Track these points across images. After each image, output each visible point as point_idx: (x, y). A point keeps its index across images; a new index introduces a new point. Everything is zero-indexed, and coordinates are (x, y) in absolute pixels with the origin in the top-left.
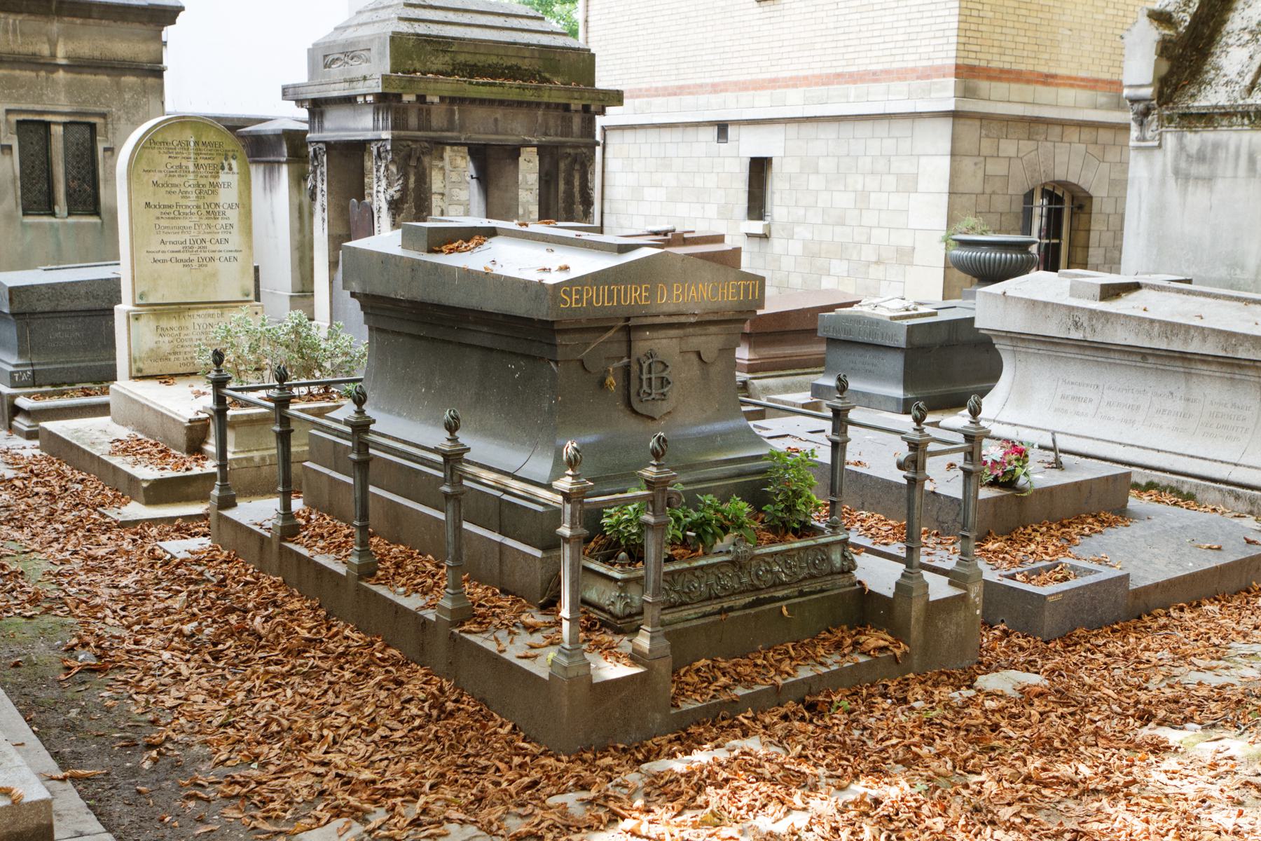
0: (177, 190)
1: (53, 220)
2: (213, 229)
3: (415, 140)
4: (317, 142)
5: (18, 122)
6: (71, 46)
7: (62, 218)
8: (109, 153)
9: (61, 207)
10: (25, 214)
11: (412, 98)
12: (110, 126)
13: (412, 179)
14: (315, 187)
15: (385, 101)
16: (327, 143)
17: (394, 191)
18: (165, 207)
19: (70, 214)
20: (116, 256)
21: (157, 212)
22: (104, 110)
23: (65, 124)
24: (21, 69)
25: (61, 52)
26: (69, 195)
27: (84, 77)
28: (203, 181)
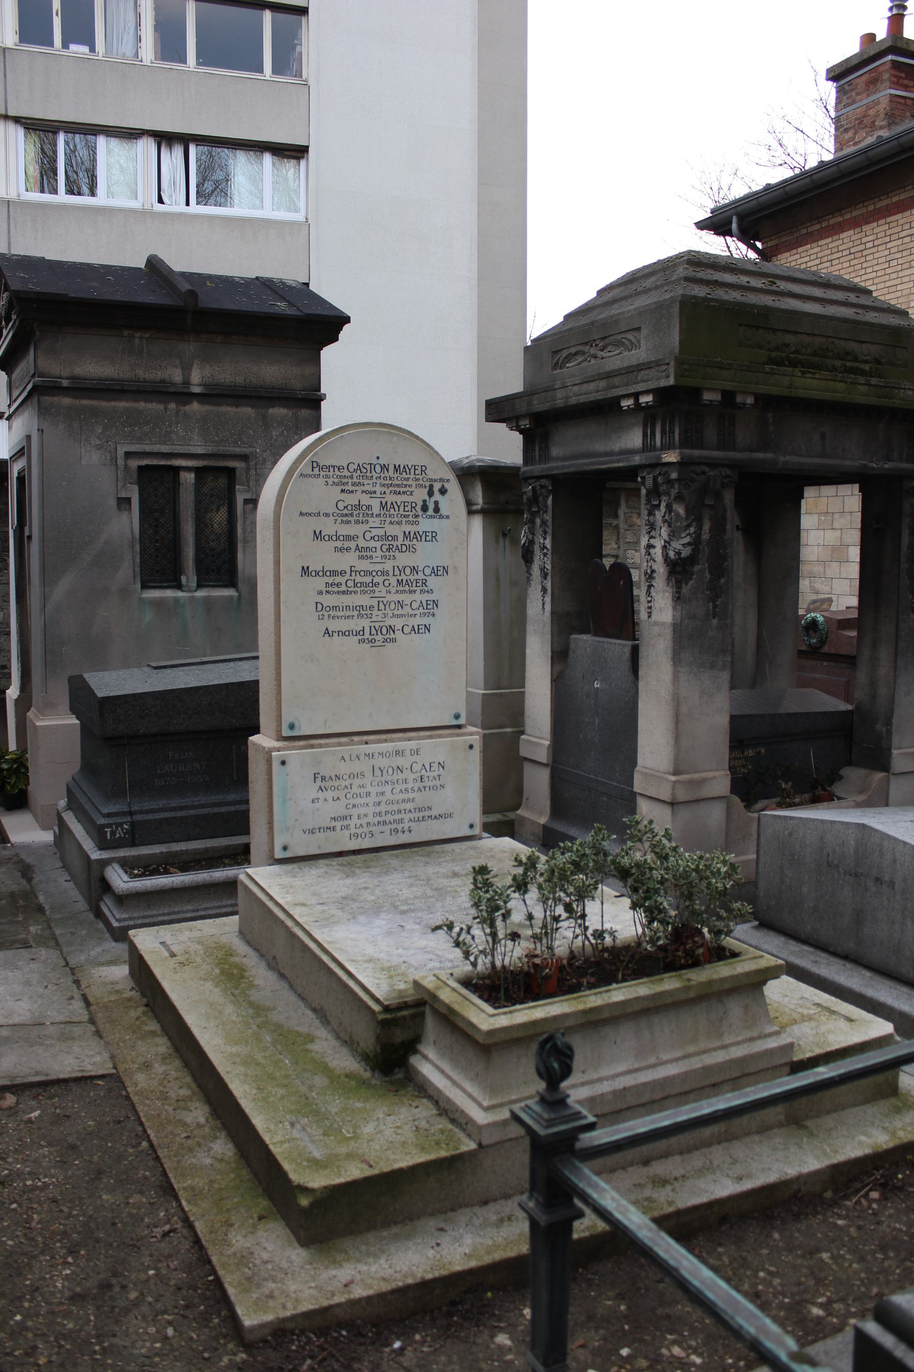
0: (352, 544)
1: (179, 594)
2: (407, 610)
3: (713, 464)
4: (538, 478)
5: (140, 468)
6: (208, 371)
7: (191, 594)
8: (250, 506)
9: (189, 577)
10: (144, 587)
11: (716, 397)
12: (253, 472)
13: (707, 526)
14: (532, 542)
15: (675, 405)
16: (553, 478)
17: (681, 546)
18: (334, 573)
19: (200, 586)
20: (254, 646)
21: (319, 583)
22: (247, 450)
23: (198, 471)
24: (146, 401)
25: (196, 377)
26: (198, 561)
27: (224, 409)
28: (393, 530)
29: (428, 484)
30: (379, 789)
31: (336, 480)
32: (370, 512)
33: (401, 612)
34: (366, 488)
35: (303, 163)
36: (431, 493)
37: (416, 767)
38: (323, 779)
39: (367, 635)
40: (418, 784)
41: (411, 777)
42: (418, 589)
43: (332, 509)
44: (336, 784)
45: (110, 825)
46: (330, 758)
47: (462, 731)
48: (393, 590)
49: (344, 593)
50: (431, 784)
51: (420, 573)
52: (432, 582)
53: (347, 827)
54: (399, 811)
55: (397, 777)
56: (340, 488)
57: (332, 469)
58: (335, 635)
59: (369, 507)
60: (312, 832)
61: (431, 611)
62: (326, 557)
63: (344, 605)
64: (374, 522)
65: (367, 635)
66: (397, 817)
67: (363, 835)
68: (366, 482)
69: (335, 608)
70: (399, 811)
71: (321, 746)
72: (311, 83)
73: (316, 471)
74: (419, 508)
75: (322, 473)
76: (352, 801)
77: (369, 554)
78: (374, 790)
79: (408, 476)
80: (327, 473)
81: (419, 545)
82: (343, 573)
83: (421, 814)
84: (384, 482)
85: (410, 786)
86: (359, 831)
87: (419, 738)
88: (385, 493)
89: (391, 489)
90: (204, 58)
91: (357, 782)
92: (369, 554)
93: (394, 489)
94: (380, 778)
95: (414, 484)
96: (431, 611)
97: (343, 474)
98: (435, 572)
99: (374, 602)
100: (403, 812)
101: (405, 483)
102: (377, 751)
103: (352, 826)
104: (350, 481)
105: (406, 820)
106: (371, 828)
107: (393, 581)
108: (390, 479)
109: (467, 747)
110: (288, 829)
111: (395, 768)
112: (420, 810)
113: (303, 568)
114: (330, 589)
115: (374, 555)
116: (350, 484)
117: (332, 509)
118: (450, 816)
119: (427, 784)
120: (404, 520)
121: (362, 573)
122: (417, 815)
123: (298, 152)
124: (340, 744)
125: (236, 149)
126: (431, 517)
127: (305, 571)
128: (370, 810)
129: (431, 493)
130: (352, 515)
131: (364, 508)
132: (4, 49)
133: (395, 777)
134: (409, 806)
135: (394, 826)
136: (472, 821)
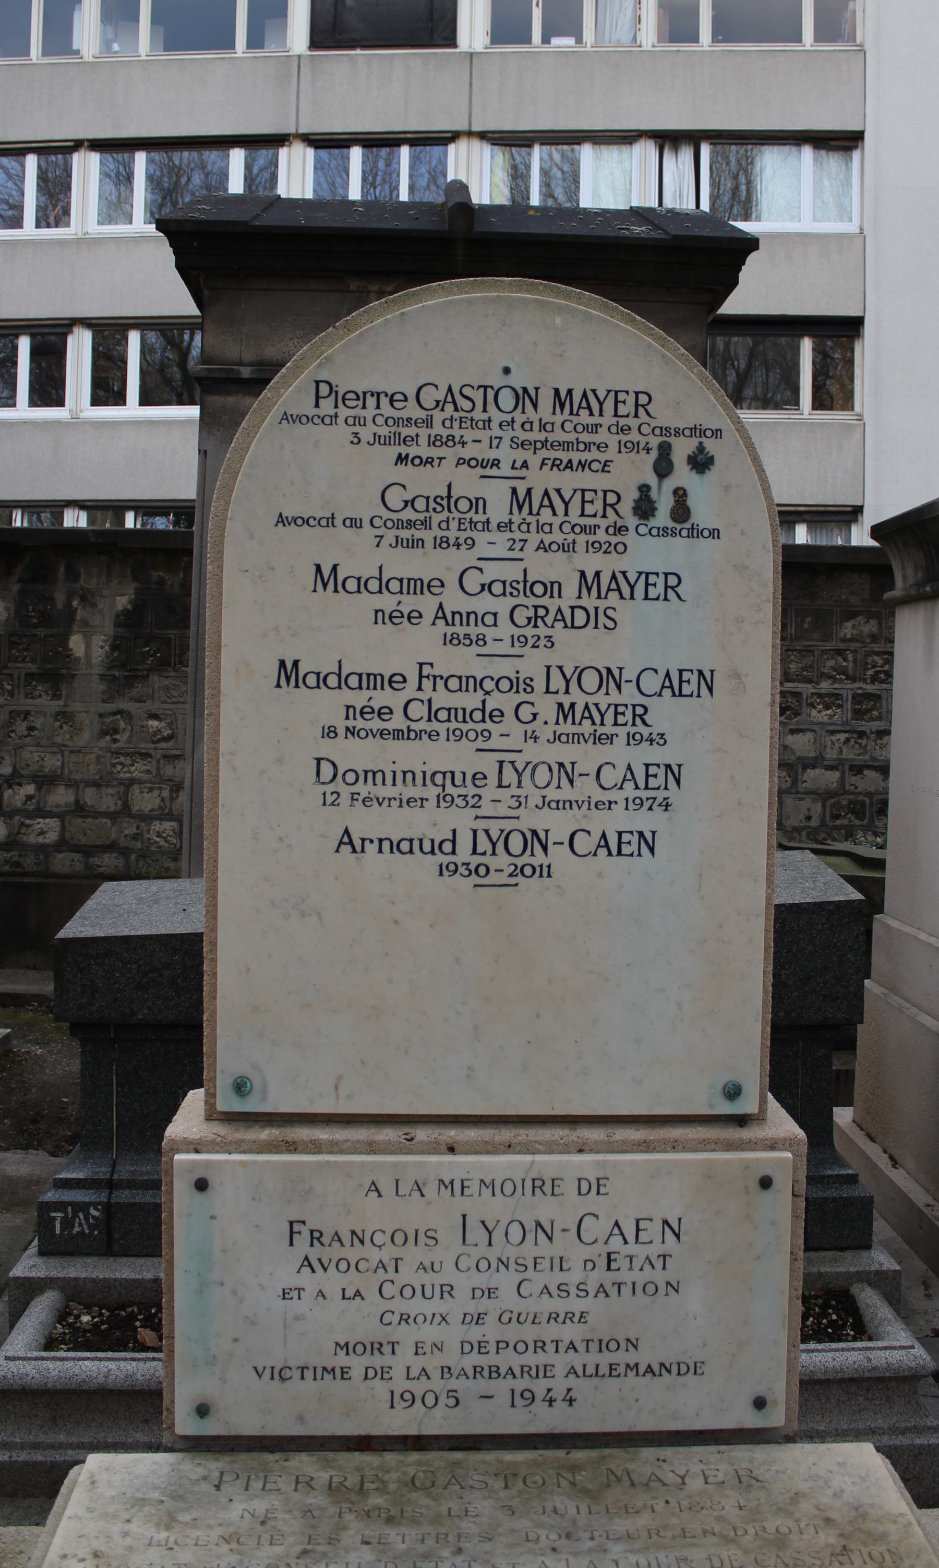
0: (427, 604)
2: (586, 788)
18: (370, 680)
21: (329, 706)
28: (544, 567)
29: (654, 442)
30: (481, 1280)
31: (384, 431)
32: (481, 517)
33: (567, 793)
34: (469, 452)
35: (856, 155)
36: (663, 468)
37: (594, 1229)
38: (316, 1237)
39: (464, 853)
40: (599, 1276)
41: (577, 1254)
42: (622, 732)
43: (368, 508)
44: (353, 1254)
45: (60, 1206)
46: (337, 1182)
47: (746, 1134)
48: (546, 733)
49: (398, 734)
50: (640, 1278)
51: (629, 689)
52: (664, 713)
53: (383, 1373)
54: (540, 1345)
55: (537, 1252)
56: (393, 451)
57: (371, 402)
58: (371, 848)
59: (477, 504)
60: (281, 1375)
61: (660, 795)
62: (348, 635)
63: (398, 769)
64: (493, 544)
65: (464, 853)
66: (531, 1359)
67: (430, 1400)
68: (469, 435)
69: (370, 775)
70: (540, 1345)
71: (316, 1147)
72: (867, 47)
73: (327, 407)
74: (626, 507)
75: (343, 412)
76: (400, 1306)
77: (473, 631)
78: (464, 1282)
79: (596, 420)
80: (358, 412)
81: (625, 611)
82: (395, 681)
83: (605, 1359)
84: (523, 436)
85: (575, 1276)
86: (418, 1388)
87: (610, 1147)
88: (525, 465)
89: (543, 453)
90: (721, 33)
91: (413, 1255)
92: (473, 631)
93: (552, 454)
94: (483, 1250)
95: (613, 441)
96: (660, 795)
97: (404, 414)
98: (674, 685)
99: (488, 764)
100: (550, 1347)
101: (585, 437)
102: (476, 1176)
103: (398, 1373)
104: (424, 432)
105: (560, 1370)
106: (454, 1384)
107: (547, 707)
108: (543, 427)
109: (754, 1184)
110: (212, 1360)
111: (530, 1225)
112: (602, 1345)
113: (282, 663)
114: (360, 723)
115: (490, 633)
116: (423, 441)
117: (368, 508)
118: (696, 1369)
119: (626, 1276)
120: (582, 539)
121: (454, 684)
122: (592, 1359)
123: (845, 142)
124: (372, 1148)
125: (763, 144)
126: (664, 532)
127: (289, 672)
128: (453, 1334)
129: (663, 468)
130: (426, 524)
131: (463, 505)
132: (472, 54)
133: (529, 1251)
134: (570, 1332)
135: (521, 1384)
136: (761, 1390)
